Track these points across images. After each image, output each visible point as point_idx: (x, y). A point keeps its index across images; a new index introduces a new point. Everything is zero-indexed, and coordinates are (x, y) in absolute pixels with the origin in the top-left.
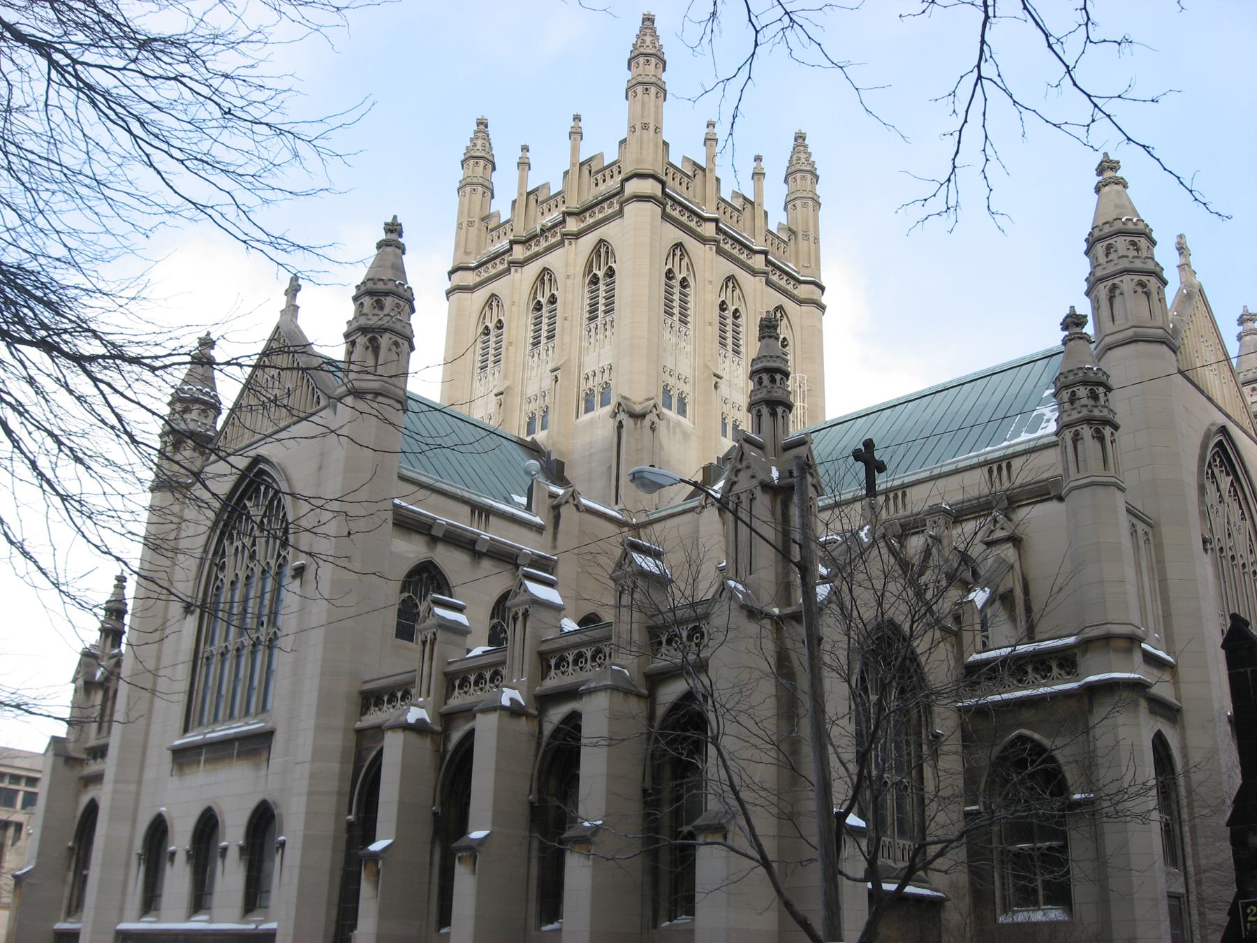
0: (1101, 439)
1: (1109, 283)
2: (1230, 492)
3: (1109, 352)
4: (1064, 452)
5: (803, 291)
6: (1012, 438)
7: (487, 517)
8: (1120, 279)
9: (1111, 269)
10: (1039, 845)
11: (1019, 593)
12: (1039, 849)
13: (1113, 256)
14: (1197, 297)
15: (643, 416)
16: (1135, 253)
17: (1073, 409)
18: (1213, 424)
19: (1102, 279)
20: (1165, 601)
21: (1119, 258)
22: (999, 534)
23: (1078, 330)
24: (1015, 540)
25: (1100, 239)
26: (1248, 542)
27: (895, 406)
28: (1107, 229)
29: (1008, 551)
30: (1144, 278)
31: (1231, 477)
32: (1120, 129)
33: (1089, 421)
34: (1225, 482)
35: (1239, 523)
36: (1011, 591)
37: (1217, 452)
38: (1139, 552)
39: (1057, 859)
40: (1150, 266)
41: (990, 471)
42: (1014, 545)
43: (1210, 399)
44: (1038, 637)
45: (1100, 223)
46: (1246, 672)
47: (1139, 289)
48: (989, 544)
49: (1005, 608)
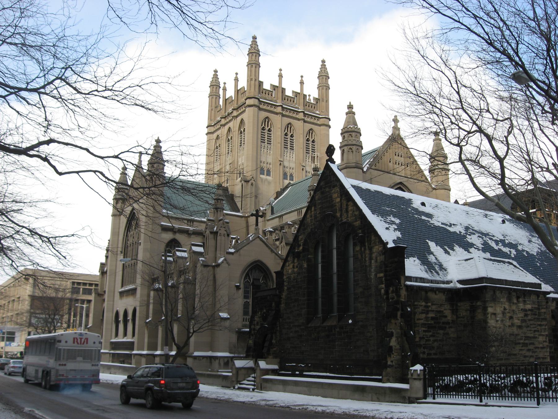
5: (321, 121)
7: (193, 223)
15: (249, 181)
30: (351, 147)
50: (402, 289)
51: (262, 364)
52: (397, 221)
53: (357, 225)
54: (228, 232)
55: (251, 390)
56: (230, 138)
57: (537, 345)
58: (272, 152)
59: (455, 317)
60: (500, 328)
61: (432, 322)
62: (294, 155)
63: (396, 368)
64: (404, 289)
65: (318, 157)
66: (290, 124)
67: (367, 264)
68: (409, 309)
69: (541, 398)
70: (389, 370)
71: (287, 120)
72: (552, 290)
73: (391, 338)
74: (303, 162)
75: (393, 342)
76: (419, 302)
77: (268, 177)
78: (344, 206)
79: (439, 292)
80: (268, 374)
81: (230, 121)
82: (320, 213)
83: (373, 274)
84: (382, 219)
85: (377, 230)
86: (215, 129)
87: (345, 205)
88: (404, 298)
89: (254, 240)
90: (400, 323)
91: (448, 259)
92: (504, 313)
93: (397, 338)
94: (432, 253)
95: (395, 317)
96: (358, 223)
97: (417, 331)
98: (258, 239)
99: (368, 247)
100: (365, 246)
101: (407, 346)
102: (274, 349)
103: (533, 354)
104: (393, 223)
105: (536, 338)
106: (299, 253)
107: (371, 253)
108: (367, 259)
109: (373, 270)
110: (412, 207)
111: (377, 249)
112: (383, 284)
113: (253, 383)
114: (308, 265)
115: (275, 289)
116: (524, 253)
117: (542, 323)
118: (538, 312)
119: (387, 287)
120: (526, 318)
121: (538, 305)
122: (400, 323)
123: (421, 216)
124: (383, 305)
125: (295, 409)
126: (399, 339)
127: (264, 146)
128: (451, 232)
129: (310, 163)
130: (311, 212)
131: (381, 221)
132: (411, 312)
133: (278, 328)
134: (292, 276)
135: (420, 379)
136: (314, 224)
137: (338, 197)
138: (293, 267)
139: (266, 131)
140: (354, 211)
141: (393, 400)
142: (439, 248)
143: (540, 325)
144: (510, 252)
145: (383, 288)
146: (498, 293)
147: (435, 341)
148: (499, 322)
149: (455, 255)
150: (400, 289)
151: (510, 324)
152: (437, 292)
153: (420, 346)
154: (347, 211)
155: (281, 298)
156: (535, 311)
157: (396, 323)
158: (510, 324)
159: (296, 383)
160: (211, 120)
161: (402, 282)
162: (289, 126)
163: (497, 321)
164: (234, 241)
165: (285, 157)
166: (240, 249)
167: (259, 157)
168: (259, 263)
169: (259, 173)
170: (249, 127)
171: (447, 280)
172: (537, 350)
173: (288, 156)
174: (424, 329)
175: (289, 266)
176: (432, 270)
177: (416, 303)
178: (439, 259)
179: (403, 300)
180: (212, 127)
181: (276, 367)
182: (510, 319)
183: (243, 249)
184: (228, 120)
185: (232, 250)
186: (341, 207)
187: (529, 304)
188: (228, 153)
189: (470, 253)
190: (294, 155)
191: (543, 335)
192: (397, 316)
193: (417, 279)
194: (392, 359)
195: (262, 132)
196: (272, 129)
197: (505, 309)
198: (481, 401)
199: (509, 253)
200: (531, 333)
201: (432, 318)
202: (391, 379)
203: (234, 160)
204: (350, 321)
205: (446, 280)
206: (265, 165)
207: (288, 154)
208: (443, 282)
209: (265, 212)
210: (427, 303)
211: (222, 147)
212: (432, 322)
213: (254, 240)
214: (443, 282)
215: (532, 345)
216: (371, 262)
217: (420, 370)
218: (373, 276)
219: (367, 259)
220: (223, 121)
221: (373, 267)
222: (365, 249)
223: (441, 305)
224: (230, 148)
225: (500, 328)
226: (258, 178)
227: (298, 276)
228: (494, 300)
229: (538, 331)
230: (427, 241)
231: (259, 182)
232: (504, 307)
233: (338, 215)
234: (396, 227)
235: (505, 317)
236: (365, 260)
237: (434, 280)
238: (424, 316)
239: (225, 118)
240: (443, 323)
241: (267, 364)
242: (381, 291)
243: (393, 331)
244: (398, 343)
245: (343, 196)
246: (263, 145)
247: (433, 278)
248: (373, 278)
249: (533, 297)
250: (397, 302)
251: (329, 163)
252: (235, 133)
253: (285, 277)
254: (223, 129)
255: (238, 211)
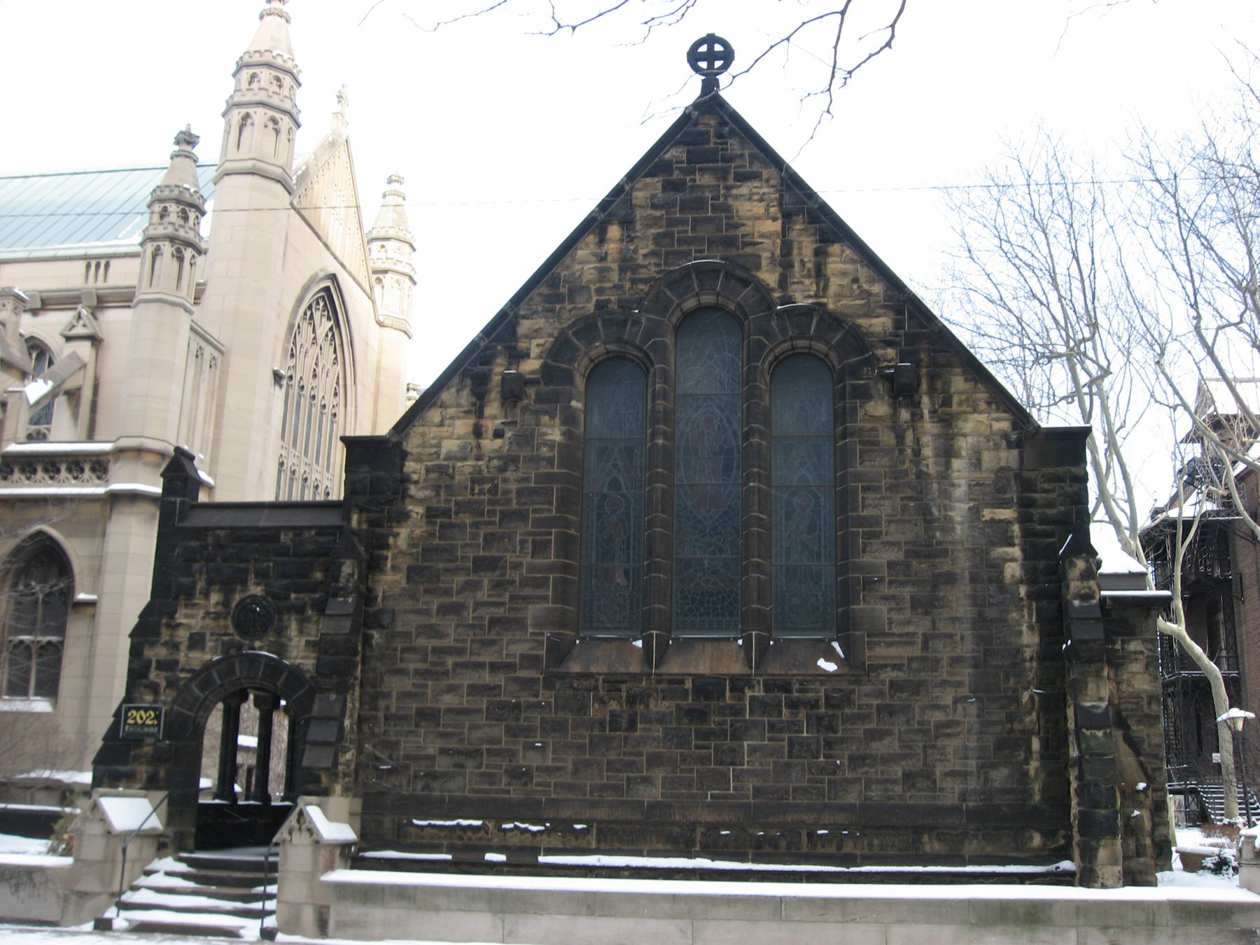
0: (181, 259)
1: (244, 111)
2: (327, 336)
3: (226, 177)
4: (142, 264)
6: (124, 238)
8: (255, 109)
9: (249, 97)
10: (40, 638)
11: (87, 394)
12: (38, 642)
13: (255, 86)
14: (343, 148)
16: (277, 89)
17: (160, 224)
18: (322, 270)
19: (238, 105)
20: (218, 425)
21: (260, 89)
22: (80, 330)
23: (188, 148)
24: (95, 340)
25: (248, 66)
26: (335, 385)
27: (28, 177)
28: (257, 58)
29: (84, 350)
30: (278, 116)
31: (332, 323)
32: (822, 17)
33: (172, 239)
34: (324, 326)
35: (329, 366)
36: (79, 389)
37: (323, 297)
38: (200, 375)
39: (52, 656)
40: (287, 105)
41: (88, 266)
42: (93, 344)
43: (326, 245)
44: (97, 437)
45: (252, 50)
46: (176, 502)
47: (271, 125)
48: (69, 339)
49: (70, 404)
96: (881, 323)
100: (917, 405)
124: (1014, 615)
145: (1013, 560)
175: (441, 424)
218: (959, 511)
222: (917, 417)
248: (958, 519)
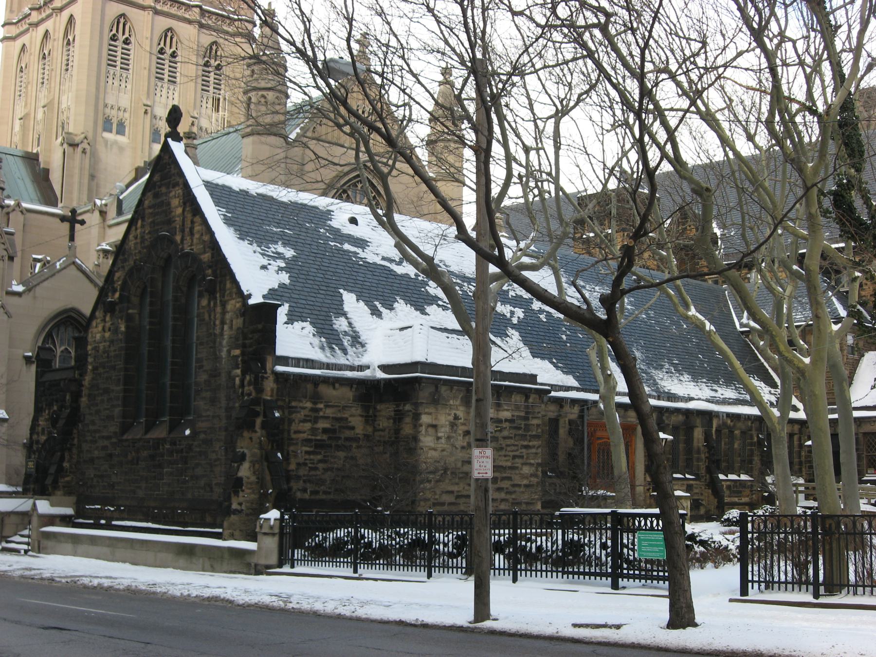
15: (77, 145)
30: (265, 93)
50: (267, 378)
51: (44, 506)
52: (289, 253)
53: (206, 260)
54: (11, 251)
55: (22, 552)
56: (46, 52)
57: (517, 480)
58: (129, 87)
59: (370, 429)
60: (443, 450)
61: (325, 437)
62: (176, 94)
63: (247, 515)
64: (271, 378)
65: (225, 99)
66: (170, 29)
67: (217, 331)
68: (277, 415)
69: (750, 581)
70: (233, 518)
71: (164, 23)
72: (575, 384)
73: (241, 464)
74: (195, 108)
75: (245, 471)
76: (300, 401)
77: (119, 138)
78: (188, 224)
79: (341, 385)
80: (52, 524)
81: (49, 17)
82: (149, 233)
83: (225, 349)
84: (259, 249)
85: (234, 271)
86: (18, 32)
87: (189, 222)
88: (269, 394)
89: (65, 268)
90: (260, 438)
91: (374, 326)
92: (453, 425)
93: (253, 463)
94: (345, 315)
95: (251, 427)
96: (206, 257)
97: (293, 451)
98: (73, 267)
99: (221, 301)
100: (215, 298)
101: (268, 478)
102: (67, 479)
103: (508, 497)
104: (279, 256)
105: (517, 468)
106: (113, 304)
107: (224, 312)
108: (218, 322)
109: (225, 342)
110: (330, 226)
111: (233, 305)
112: (238, 368)
113: (26, 540)
114: (127, 327)
115: (72, 368)
116: (541, 316)
117: (531, 444)
118: (525, 425)
119: (244, 373)
120: (497, 434)
121: (527, 413)
122: (260, 438)
123: (341, 244)
125: (60, 582)
126: (257, 466)
127: (114, 74)
128: (398, 275)
129: (209, 111)
130: (136, 229)
131: (255, 252)
132: (281, 419)
133: (76, 441)
134: (101, 346)
135: (274, 535)
136: (140, 252)
137: (180, 206)
138: (104, 330)
139: (119, 43)
140: (202, 235)
141: (233, 569)
142: (362, 303)
143: (527, 447)
144: (512, 313)
145: (238, 376)
146: (443, 389)
147: (326, 470)
148: (443, 441)
149: (391, 319)
150: (263, 378)
151: (465, 444)
152: (337, 385)
153: (298, 478)
154: (192, 234)
155: (82, 386)
156: (519, 422)
157: (251, 438)
158: (465, 444)
159: (93, 540)
160: (11, 11)
161: (269, 365)
162: (169, 34)
163: (438, 438)
164: (38, 265)
165: (157, 98)
166: (36, 286)
167: (101, 96)
168: (73, 314)
169: (100, 129)
170: (82, 33)
171: (360, 363)
172: (517, 489)
173: (164, 96)
174: (308, 449)
176: (334, 346)
177: (293, 404)
178: (355, 324)
179: (269, 398)
180: (13, 28)
181: (69, 511)
182: (464, 435)
183: (41, 285)
184: (44, 15)
185: (20, 288)
186: (183, 225)
187: (507, 410)
188: (43, 83)
189: (426, 314)
190: (176, 94)
191: (531, 465)
192: (254, 426)
193: (298, 362)
194: (241, 499)
195: (110, 45)
196: (132, 39)
197: (456, 418)
198: (355, 571)
199: (508, 315)
200: (507, 461)
201: (325, 431)
202: (237, 533)
203: (54, 99)
204: (188, 432)
205: (357, 363)
206: (114, 112)
207: (165, 91)
208: (352, 368)
209: (104, 209)
210: (315, 403)
211: (31, 69)
212: (325, 437)
213: (65, 268)
214: (352, 368)
215: (506, 482)
216: (223, 329)
217: (275, 520)
218: (224, 354)
219: (218, 322)
220: (35, 17)
221: (226, 337)
222: (215, 304)
223: (344, 408)
224: (47, 72)
225: (443, 450)
226: (99, 139)
227: (109, 346)
228: (436, 401)
229: (521, 457)
230: (341, 291)
231: (101, 149)
232: (455, 414)
233: (178, 238)
234: (283, 265)
235: (455, 432)
236: (214, 324)
237: (333, 364)
238: (308, 426)
239: (39, 9)
240: (347, 439)
241: (52, 505)
242: (234, 380)
243: (246, 451)
244: (254, 473)
245: (188, 204)
246: (112, 72)
247: (332, 360)
249: (517, 399)
250: (257, 401)
251: (169, 140)
252: (56, 43)
253: (89, 347)
254: (34, 33)
255: (55, 204)
